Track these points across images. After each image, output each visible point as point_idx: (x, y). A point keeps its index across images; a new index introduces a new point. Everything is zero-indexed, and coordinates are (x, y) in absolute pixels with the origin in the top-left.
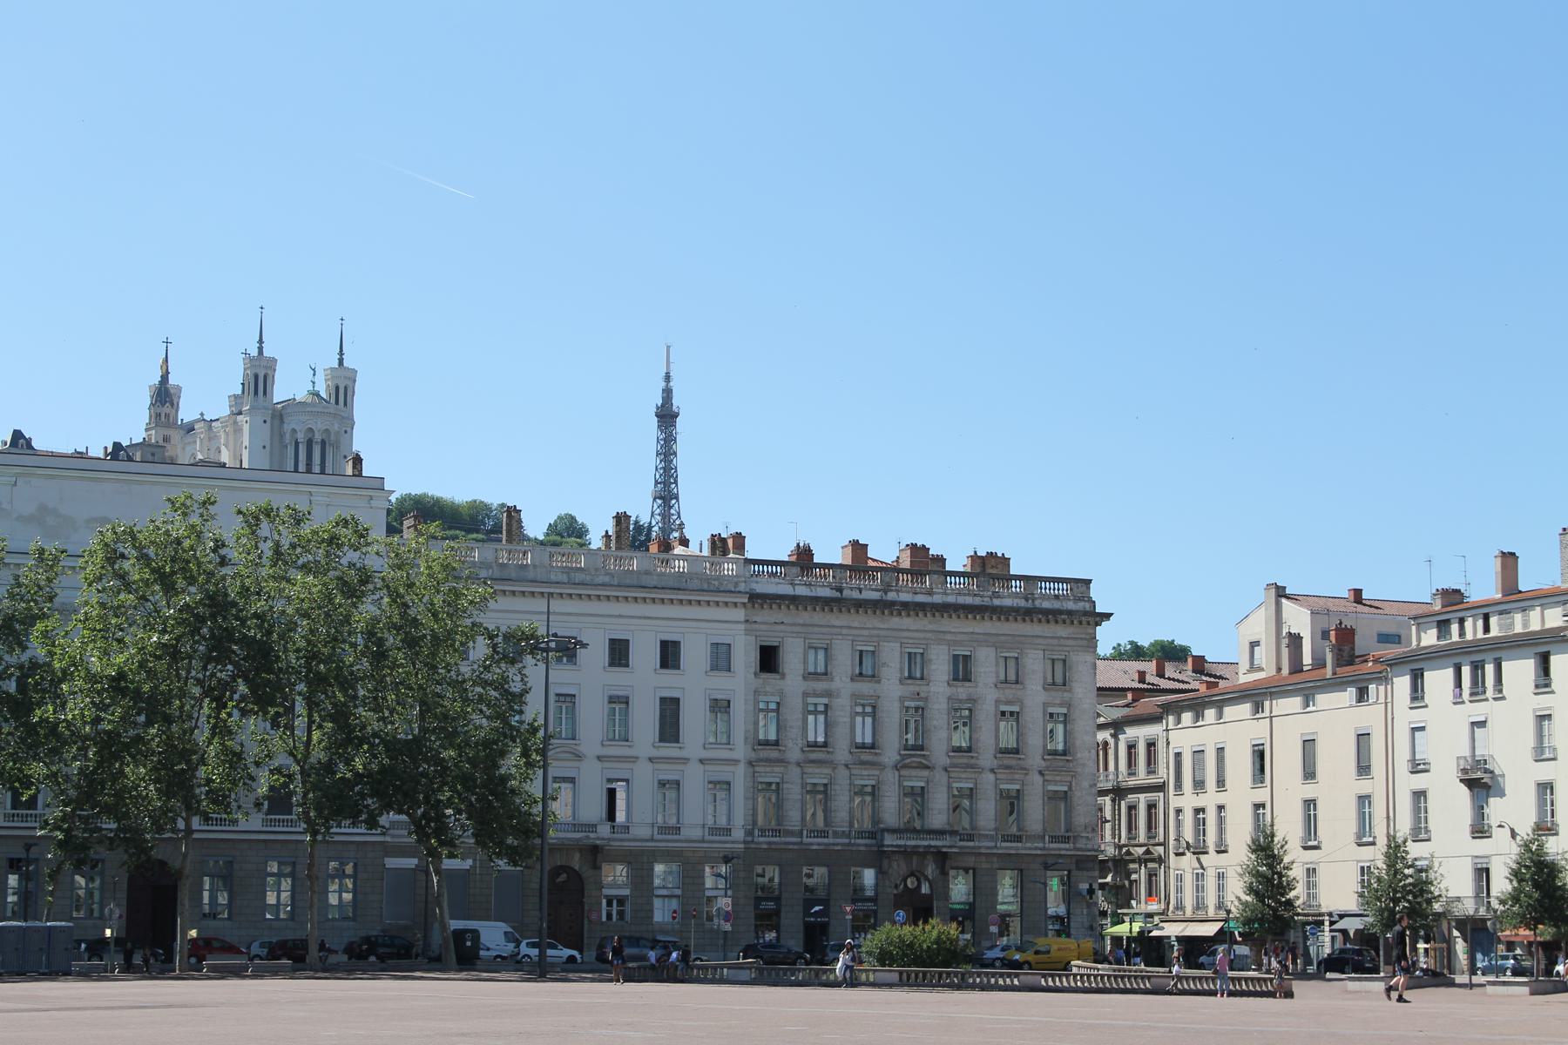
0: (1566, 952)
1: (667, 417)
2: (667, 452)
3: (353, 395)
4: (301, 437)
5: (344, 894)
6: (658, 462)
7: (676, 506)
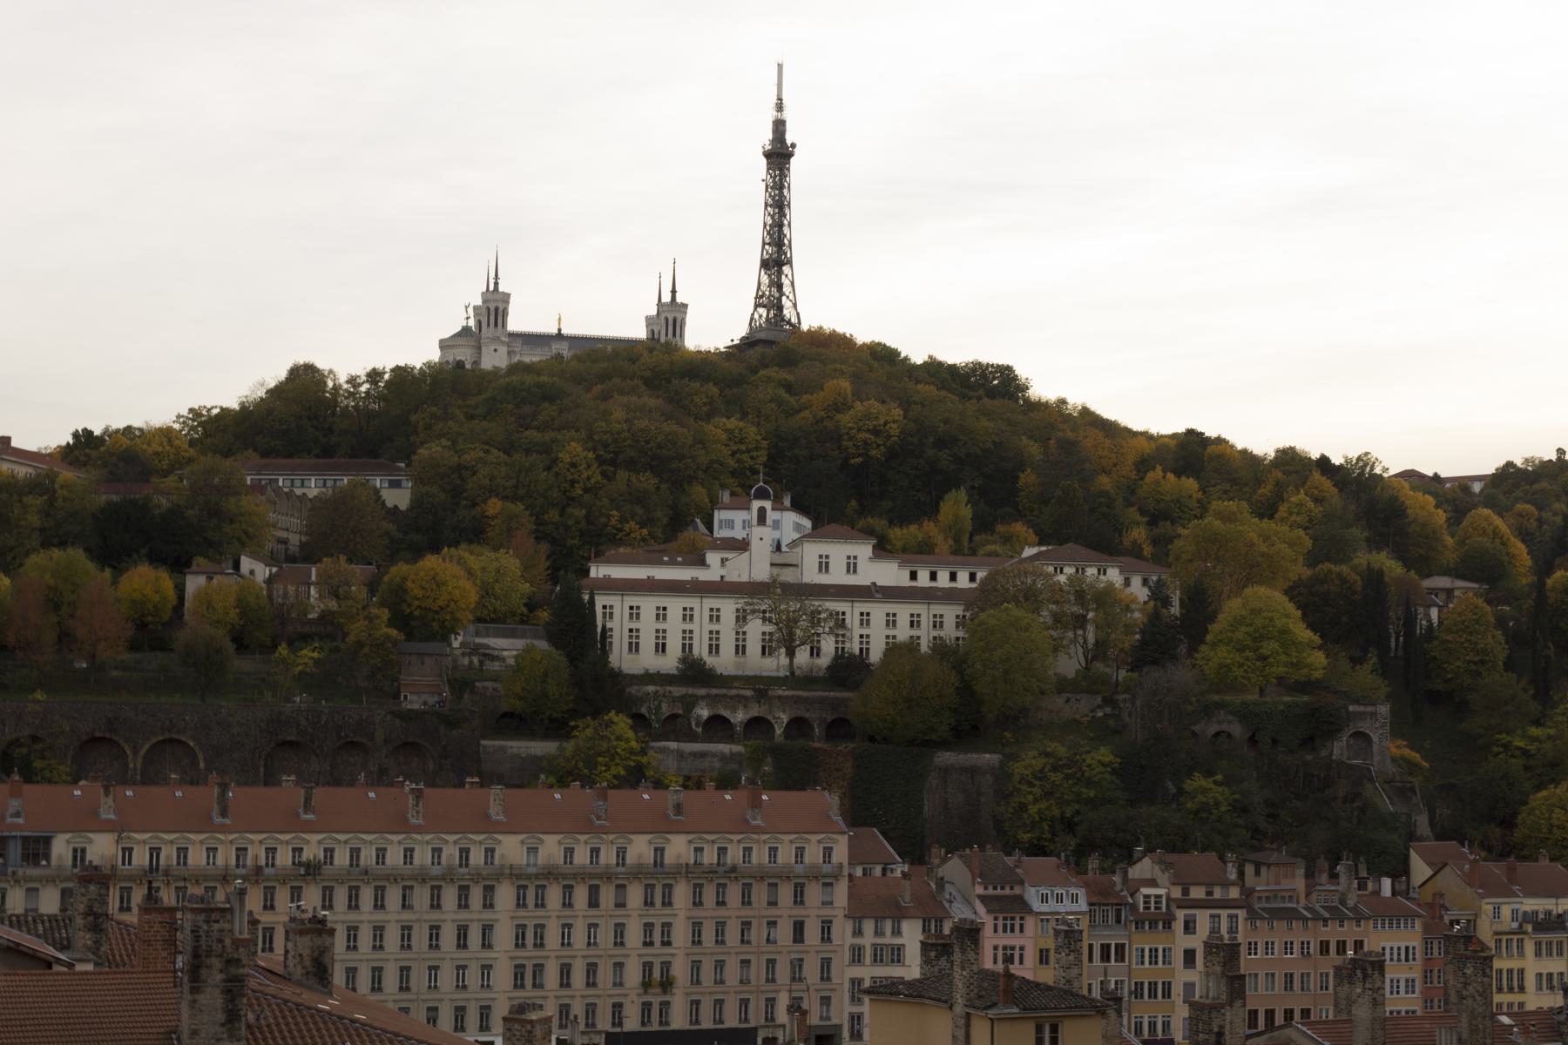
0: (640, 1032)
1: (779, 155)
2: (778, 204)
5: (1277, 1024)
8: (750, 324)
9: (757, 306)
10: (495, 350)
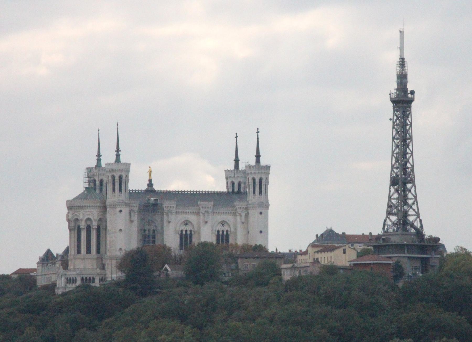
8: (384, 228)
9: (389, 214)
10: (121, 211)
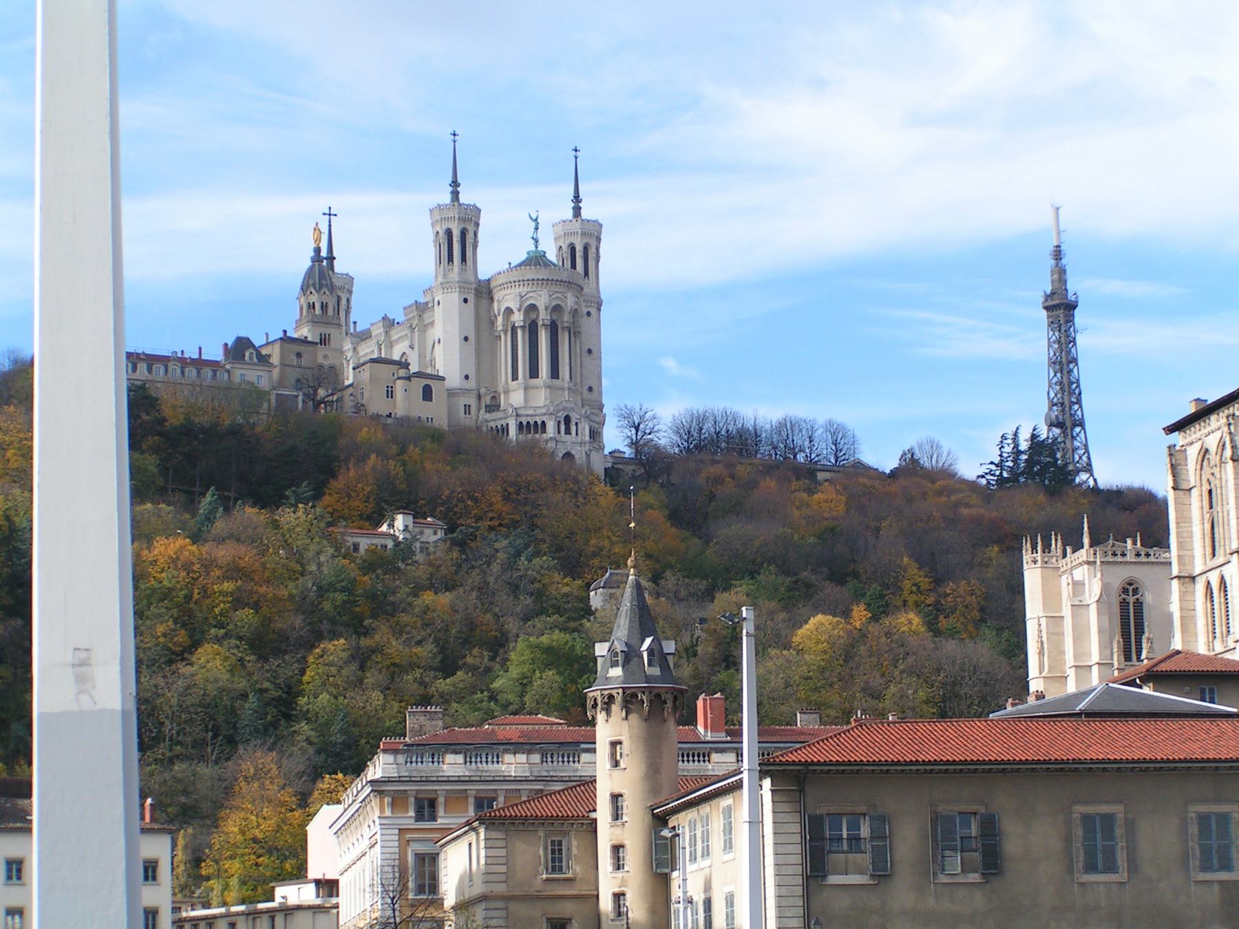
3: (598, 261)
4: (518, 318)
6: (1052, 374)
7: (1082, 435)
